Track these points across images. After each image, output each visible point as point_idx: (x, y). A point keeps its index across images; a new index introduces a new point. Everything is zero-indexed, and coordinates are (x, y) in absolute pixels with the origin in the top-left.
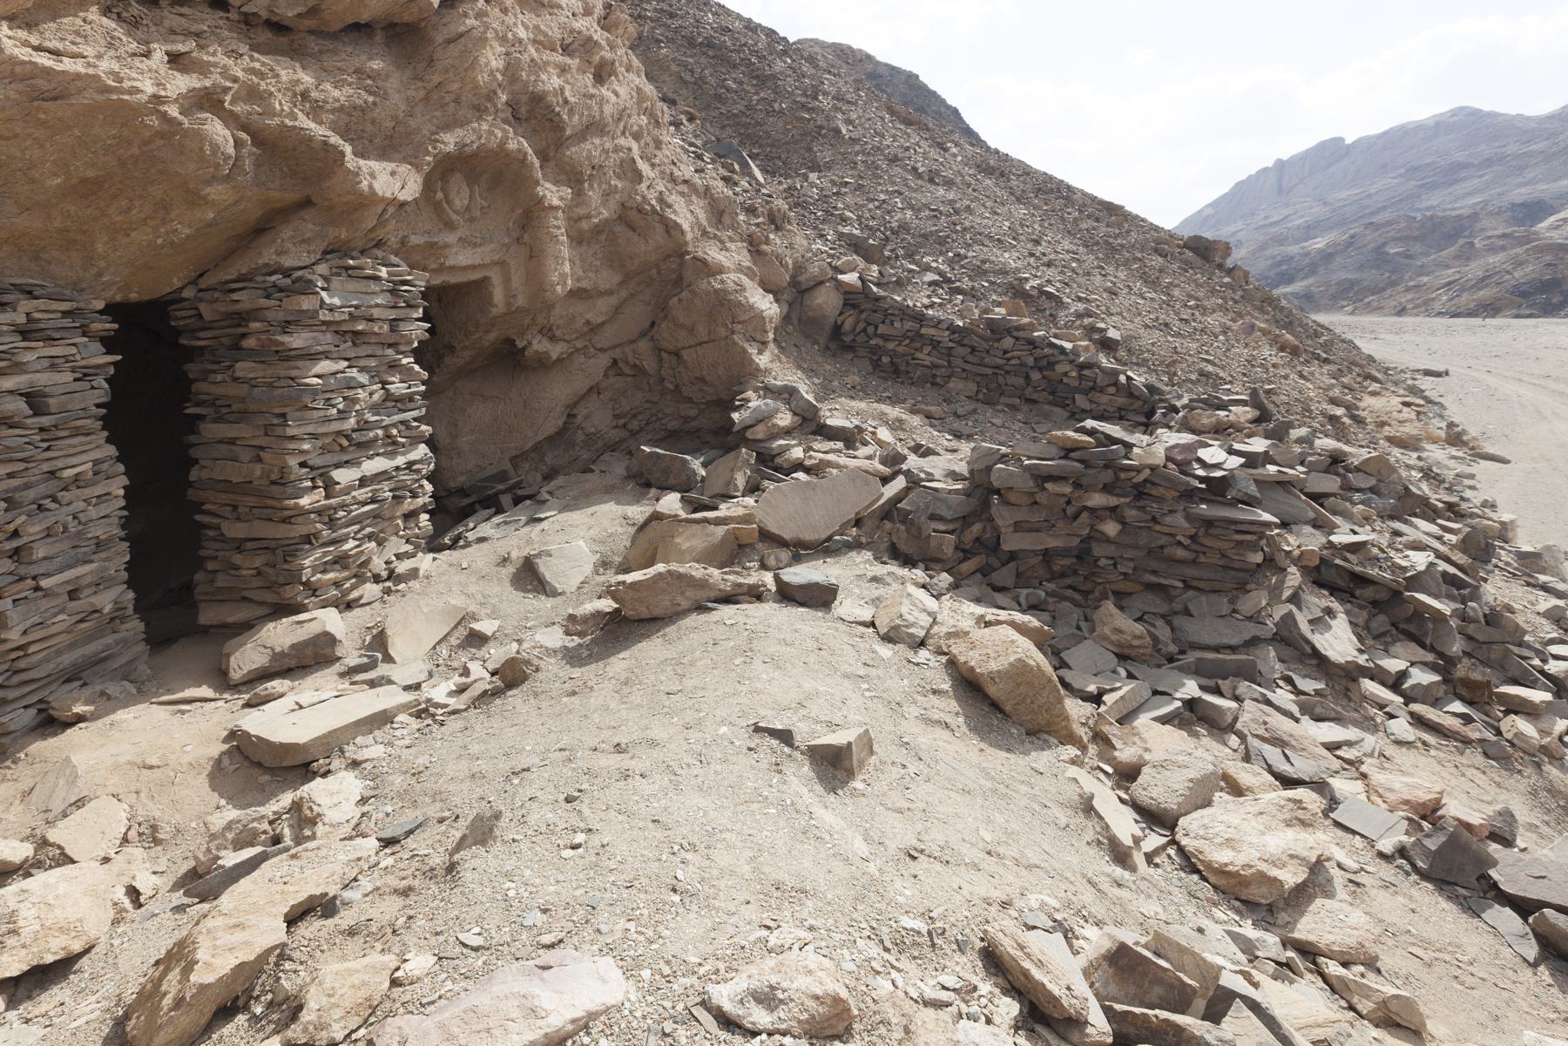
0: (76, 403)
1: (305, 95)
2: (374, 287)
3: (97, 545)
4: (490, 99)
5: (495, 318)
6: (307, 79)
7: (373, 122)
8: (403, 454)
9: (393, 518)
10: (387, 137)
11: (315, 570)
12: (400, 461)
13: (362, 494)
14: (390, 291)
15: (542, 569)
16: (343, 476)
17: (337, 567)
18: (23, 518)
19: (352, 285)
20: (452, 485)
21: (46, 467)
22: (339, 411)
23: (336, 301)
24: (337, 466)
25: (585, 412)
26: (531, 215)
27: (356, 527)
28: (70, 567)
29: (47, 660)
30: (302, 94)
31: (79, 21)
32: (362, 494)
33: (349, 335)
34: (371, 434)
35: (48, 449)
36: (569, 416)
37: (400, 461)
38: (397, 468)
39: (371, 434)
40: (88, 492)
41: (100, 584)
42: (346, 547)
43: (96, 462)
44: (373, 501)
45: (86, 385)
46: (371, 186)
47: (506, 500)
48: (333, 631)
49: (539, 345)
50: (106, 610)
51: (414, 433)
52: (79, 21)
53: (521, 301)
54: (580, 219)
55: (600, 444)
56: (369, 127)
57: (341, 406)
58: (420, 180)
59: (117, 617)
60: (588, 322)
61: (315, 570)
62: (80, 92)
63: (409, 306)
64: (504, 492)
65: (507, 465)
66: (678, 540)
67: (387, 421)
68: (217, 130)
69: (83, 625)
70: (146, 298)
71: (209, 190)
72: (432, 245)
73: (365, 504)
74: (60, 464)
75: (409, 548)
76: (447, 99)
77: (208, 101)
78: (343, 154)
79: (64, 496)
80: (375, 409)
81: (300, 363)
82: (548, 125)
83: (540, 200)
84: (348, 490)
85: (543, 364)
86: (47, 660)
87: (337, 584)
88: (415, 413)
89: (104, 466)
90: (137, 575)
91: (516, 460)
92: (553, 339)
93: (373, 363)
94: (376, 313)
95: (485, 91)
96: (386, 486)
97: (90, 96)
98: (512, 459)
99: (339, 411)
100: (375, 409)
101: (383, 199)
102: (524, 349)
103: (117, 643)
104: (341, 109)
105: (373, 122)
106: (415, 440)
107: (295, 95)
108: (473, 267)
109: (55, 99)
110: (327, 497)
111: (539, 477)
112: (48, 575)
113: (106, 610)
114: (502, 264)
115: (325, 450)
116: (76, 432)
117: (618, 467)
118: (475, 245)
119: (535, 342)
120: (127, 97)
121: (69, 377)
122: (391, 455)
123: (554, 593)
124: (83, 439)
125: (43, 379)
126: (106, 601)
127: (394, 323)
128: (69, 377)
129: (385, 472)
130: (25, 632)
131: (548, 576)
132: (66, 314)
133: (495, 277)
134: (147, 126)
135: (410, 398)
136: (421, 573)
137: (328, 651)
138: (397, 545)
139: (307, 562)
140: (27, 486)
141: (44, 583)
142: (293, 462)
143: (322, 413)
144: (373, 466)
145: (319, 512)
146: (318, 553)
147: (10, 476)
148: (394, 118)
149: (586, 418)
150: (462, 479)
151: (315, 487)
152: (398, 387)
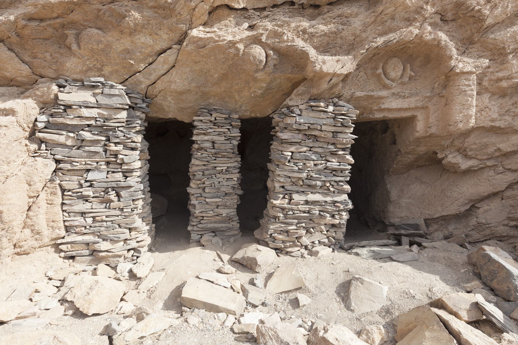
0: (223, 147)
1: (304, 31)
2: (322, 115)
3: (226, 194)
4: (418, 13)
5: (418, 139)
6: (305, 24)
7: (341, 38)
8: (332, 197)
9: (319, 224)
10: (350, 45)
11: (275, 231)
12: (329, 199)
13: (306, 208)
14: (334, 118)
15: (352, 289)
16: (296, 197)
17: (286, 234)
18: (206, 179)
19: (312, 114)
20: (392, 221)
21: (212, 165)
22: (299, 169)
23: (302, 121)
24: (297, 192)
25: (486, 207)
26: (449, 77)
27: (296, 221)
28: (215, 198)
29: (207, 223)
30: (295, 31)
31: (228, 21)
32: (306, 208)
33: (309, 135)
34: (314, 183)
35: (215, 160)
36: (473, 206)
37: (329, 199)
38: (326, 202)
39: (314, 183)
40: (224, 176)
41: (225, 206)
42: (290, 228)
43: (228, 167)
44: (309, 212)
45: (229, 142)
46: (321, 68)
47: (405, 240)
48: (257, 260)
49: (453, 158)
50: (224, 215)
51: (340, 188)
52: (228, 21)
53: (433, 130)
54: (500, 80)
55: (488, 232)
56: (339, 41)
57: (300, 167)
58: (355, 64)
59: (229, 219)
60: (499, 149)
61: (275, 231)
62: (209, 43)
63: (343, 125)
64: (406, 235)
65: (422, 222)
66: (427, 334)
67: (324, 178)
68: (259, 52)
69: (218, 217)
70: (263, 116)
71: (257, 75)
72: (371, 97)
73: (304, 212)
74: (216, 165)
75: (326, 240)
76: (386, 18)
77: (257, 40)
78: (305, 55)
79: (218, 175)
80: (319, 172)
81: (285, 145)
82: (471, 20)
83: (452, 69)
84: (297, 204)
85: (454, 171)
86: (207, 223)
87: (283, 242)
88: (342, 179)
89: (230, 169)
90: (240, 209)
91: (428, 222)
92: (466, 157)
93: (320, 150)
94: (324, 127)
95: (413, 8)
96: (317, 208)
97: (212, 44)
98: (425, 220)
99: (299, 169)
100: (319, 172)
101: (328, 74)
102: (443, 159)
103: (226, 227)
104: (325, 35)
105: (341, 38)
106: (341, 192)
107: (298, 32)
108: (406, 109)
109: (203, 47)
110: (289, 203)
111: (441, 236)
112: (208, 198)
113: (224, 215)
114: (424, 108)
115: (294, 184)
116: (224, 157)
117: (460, 255)
118: (404, 97)
119: (450, 156)
120: (220, 43)
121: (223, 138)
122: (325, 195)
123: (348, 307)
124: (226, 159)
125: (216, 138)
126: (224, 212)
127: (335, 134)
128: (223, 138)
129: (318, 201)
130: (201, 212)
131: (352, 295)
132: (226, 119)
133: (420, 116)
134: (231, 53)
135: (342, 171)
136: (319, 255)
137: (254, 266)
138: (317, 237)
139: (272, 227)
140: (207, 170)
141: (207, 200)
142: (277, 185)
143: (290, 168)
144: (311, 197)
145: (283, 209)
146: (277, 225)
147: (204, 165)
148: (354, 34)
149: (486, 211)
150: (397, 220)
151: (284, 198)
152: (334, 163)
